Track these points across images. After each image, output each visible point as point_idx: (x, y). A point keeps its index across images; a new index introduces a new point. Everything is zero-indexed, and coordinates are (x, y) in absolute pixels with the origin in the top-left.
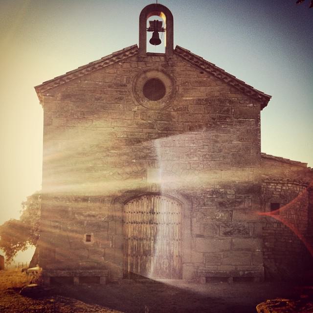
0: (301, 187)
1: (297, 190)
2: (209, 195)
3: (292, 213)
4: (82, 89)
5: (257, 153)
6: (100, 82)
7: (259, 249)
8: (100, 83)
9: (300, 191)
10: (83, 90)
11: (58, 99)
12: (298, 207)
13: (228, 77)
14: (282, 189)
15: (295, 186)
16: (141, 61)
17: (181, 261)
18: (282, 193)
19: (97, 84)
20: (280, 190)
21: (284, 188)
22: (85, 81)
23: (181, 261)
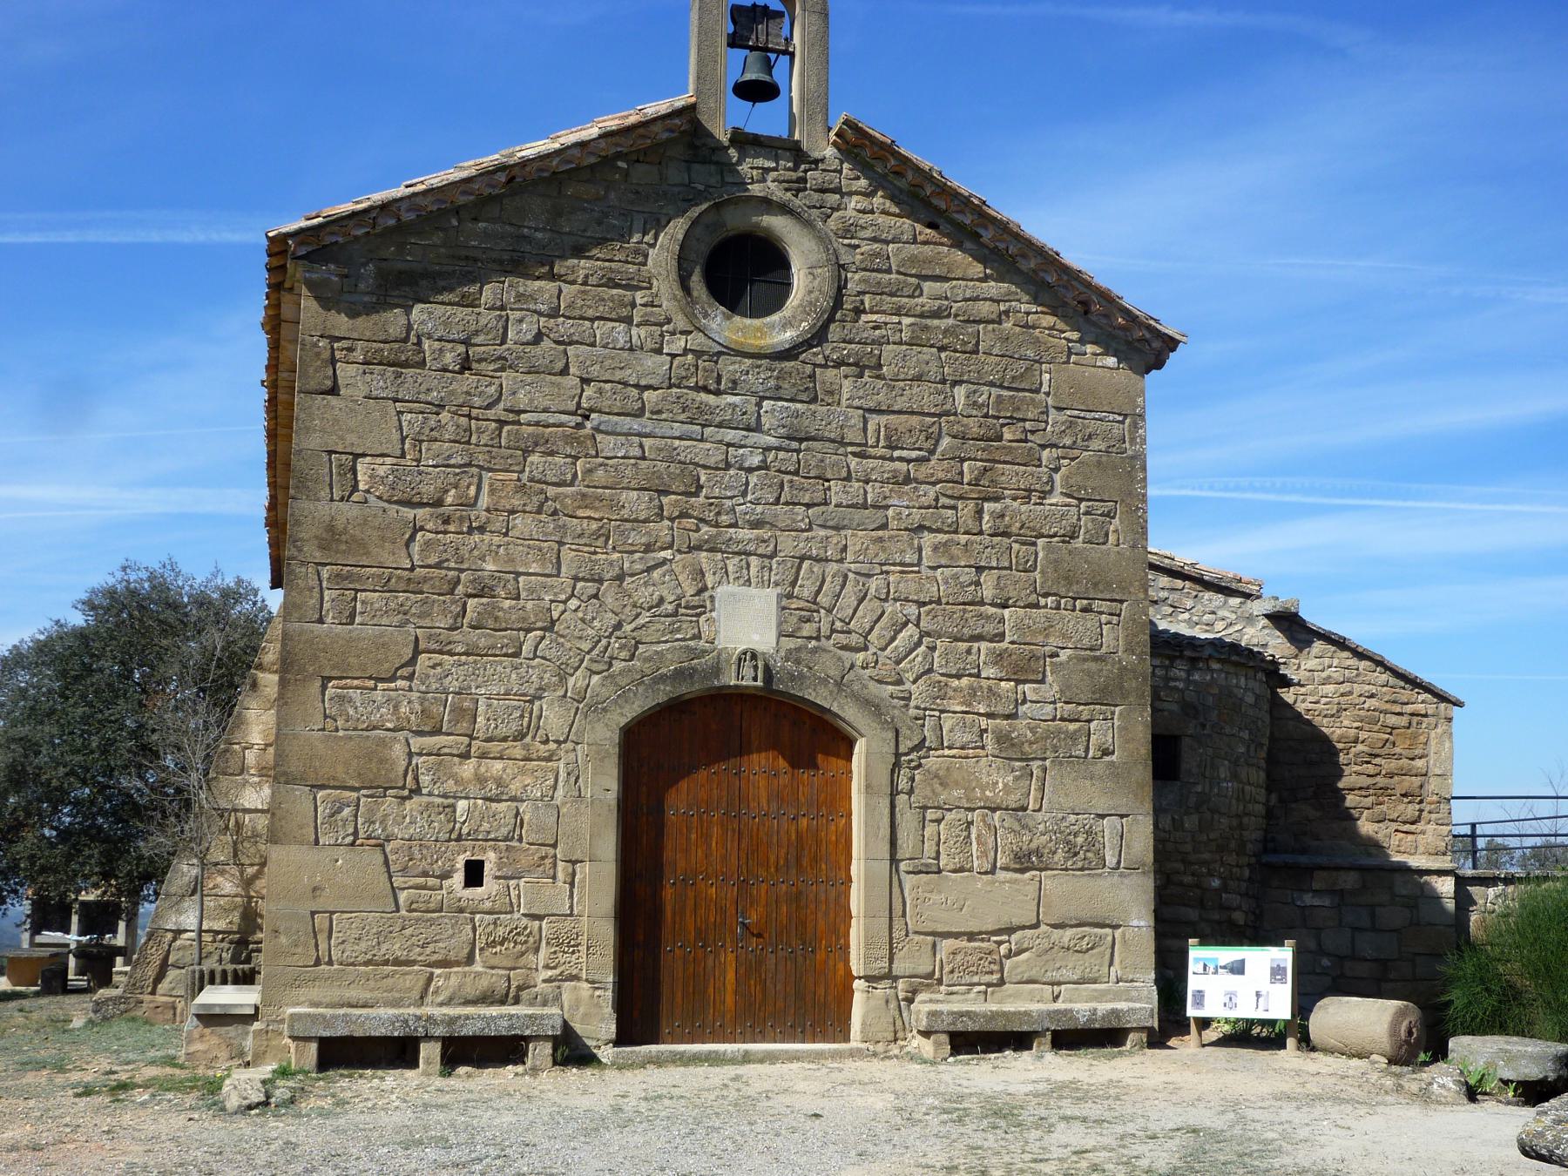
0: (1251, 673)
1: (1237, 686)
2: (962, 703)
3: (1223, 776)
4: (464, 253)
5: (1134, 547)
6: (536, 230)
7: (1139, 919)
8: (539, 235)
9: (1246, 689)
10: (467, 258)
11: (362, 286)
12: (1242, 750)
13: (1031, 254)
14: (1188, 681)
15: (1232, 670)
16: (704, 162)
17: (432, 1106)
18: (1190, 696)
19: (524, 237)
20: (1181, 685)
21: (1196, 677)
22: (475, 219)
23: (432, 1106)
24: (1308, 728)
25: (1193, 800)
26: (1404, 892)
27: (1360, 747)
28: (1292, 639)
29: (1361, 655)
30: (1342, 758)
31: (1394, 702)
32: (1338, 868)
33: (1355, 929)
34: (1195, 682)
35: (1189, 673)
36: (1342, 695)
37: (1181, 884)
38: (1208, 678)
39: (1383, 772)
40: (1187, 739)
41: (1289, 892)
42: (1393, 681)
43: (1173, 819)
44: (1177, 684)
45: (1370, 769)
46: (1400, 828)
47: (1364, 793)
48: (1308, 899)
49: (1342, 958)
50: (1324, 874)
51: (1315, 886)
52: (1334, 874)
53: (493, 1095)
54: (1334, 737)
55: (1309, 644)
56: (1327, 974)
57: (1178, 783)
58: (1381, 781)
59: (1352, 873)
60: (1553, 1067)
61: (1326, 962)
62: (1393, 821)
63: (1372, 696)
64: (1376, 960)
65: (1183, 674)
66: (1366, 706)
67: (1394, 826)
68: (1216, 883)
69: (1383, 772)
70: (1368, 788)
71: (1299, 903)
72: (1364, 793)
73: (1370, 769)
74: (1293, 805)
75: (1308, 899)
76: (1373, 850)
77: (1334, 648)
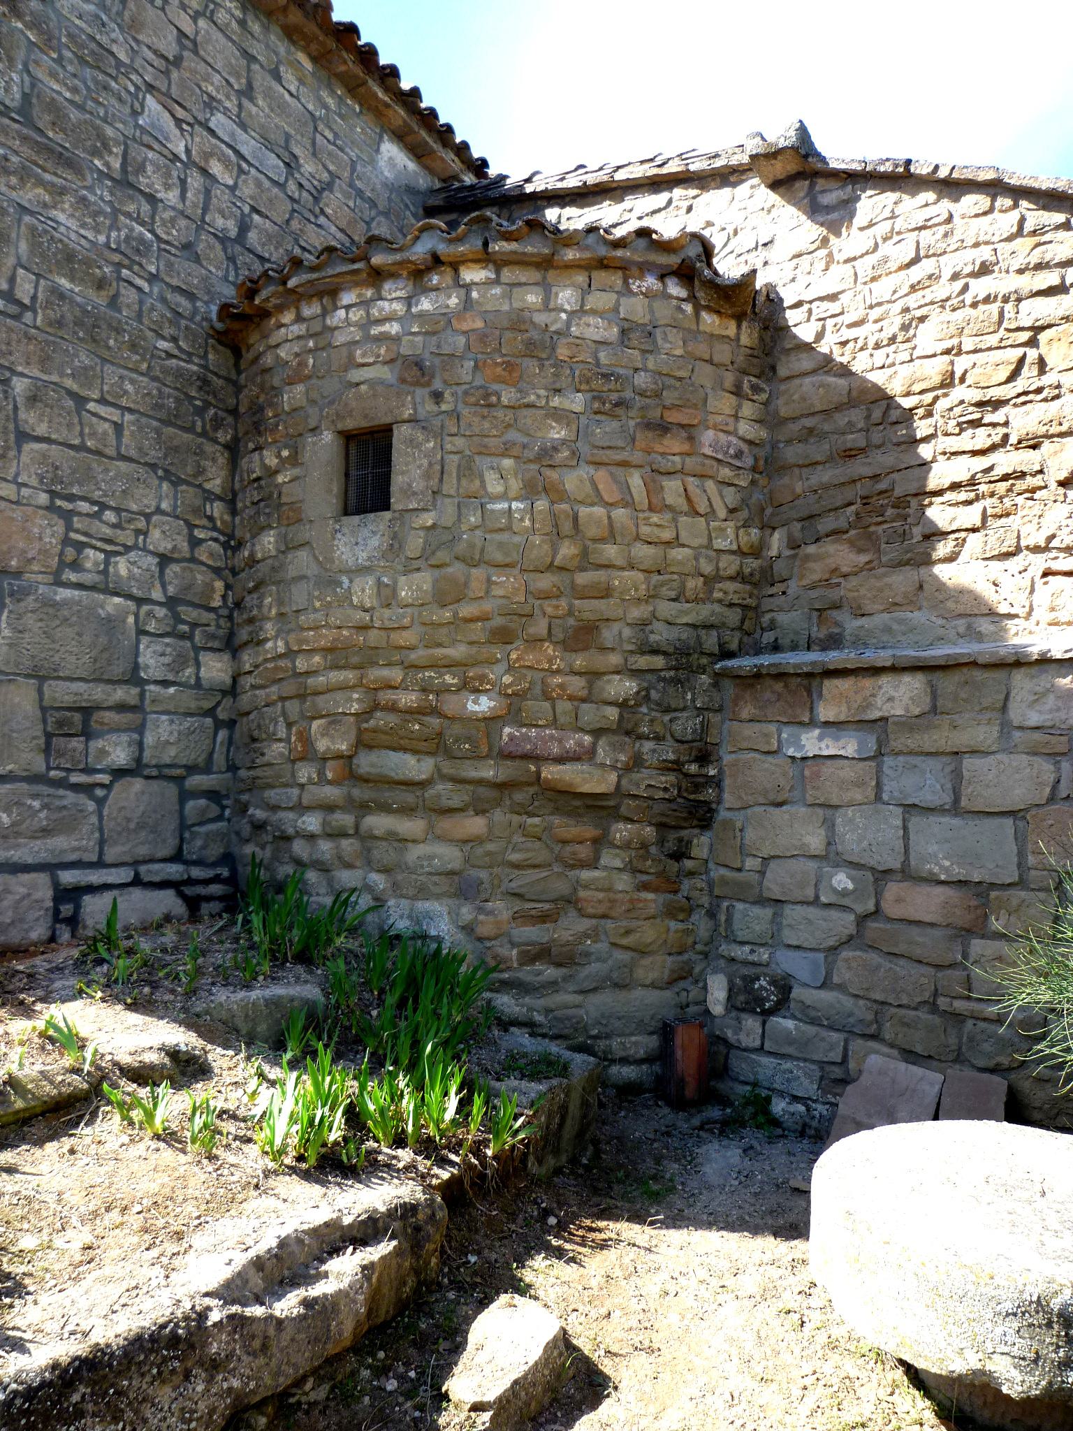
20: (394, 328)
21: (425, 304)
24: (842, 382)
25: (415, 544)
26: (1034, 719)
27: (958, 393)
28: (814, 210)
29: (952, 187)
30: (922, 428)
31: (1039, 267)
32: (876, 671)
33: (910, 808)
34: (421, 315)
35: (409, 301)
36: (913, 289)
37: (393, 708)
38: (453, 301)
39: (1013, 439)
40: (404, 427)
41: (772, 728)
42: (1036, 217)
43: (379, 583)
44: (386, 328)
45: (981, 438)
46: (1056, 566)
47: (963, 496)
48: (812, 743)
49: (882, 876)
50: (843, 685)
51: (825, 712)
52: (867, 683)
53: (664, 936)
54: (895, 387)
55: (847, 208)
56: (844, 908)
57: (387, 515)
58: (1005, 461)
59: (907, 678)
60: (1022, 1346)
61: (842, 880)
62: (1036, 549)
63: (984, 270)
64: (961, 883)
65: (398, 307)
66: (968, 298)
67: (1039, 562)
68: (483, 705)
69: (1013, 439)
70: (972, 482)
71: (791, 752)
72: (963, 496)
73: (981, 438)
74: (811, 549)
75: (812, 743)
76: (985, 626)
77: (891, 196)
